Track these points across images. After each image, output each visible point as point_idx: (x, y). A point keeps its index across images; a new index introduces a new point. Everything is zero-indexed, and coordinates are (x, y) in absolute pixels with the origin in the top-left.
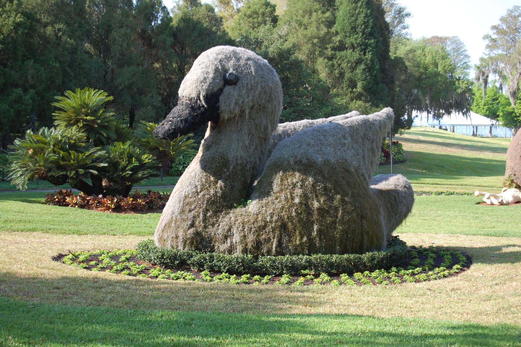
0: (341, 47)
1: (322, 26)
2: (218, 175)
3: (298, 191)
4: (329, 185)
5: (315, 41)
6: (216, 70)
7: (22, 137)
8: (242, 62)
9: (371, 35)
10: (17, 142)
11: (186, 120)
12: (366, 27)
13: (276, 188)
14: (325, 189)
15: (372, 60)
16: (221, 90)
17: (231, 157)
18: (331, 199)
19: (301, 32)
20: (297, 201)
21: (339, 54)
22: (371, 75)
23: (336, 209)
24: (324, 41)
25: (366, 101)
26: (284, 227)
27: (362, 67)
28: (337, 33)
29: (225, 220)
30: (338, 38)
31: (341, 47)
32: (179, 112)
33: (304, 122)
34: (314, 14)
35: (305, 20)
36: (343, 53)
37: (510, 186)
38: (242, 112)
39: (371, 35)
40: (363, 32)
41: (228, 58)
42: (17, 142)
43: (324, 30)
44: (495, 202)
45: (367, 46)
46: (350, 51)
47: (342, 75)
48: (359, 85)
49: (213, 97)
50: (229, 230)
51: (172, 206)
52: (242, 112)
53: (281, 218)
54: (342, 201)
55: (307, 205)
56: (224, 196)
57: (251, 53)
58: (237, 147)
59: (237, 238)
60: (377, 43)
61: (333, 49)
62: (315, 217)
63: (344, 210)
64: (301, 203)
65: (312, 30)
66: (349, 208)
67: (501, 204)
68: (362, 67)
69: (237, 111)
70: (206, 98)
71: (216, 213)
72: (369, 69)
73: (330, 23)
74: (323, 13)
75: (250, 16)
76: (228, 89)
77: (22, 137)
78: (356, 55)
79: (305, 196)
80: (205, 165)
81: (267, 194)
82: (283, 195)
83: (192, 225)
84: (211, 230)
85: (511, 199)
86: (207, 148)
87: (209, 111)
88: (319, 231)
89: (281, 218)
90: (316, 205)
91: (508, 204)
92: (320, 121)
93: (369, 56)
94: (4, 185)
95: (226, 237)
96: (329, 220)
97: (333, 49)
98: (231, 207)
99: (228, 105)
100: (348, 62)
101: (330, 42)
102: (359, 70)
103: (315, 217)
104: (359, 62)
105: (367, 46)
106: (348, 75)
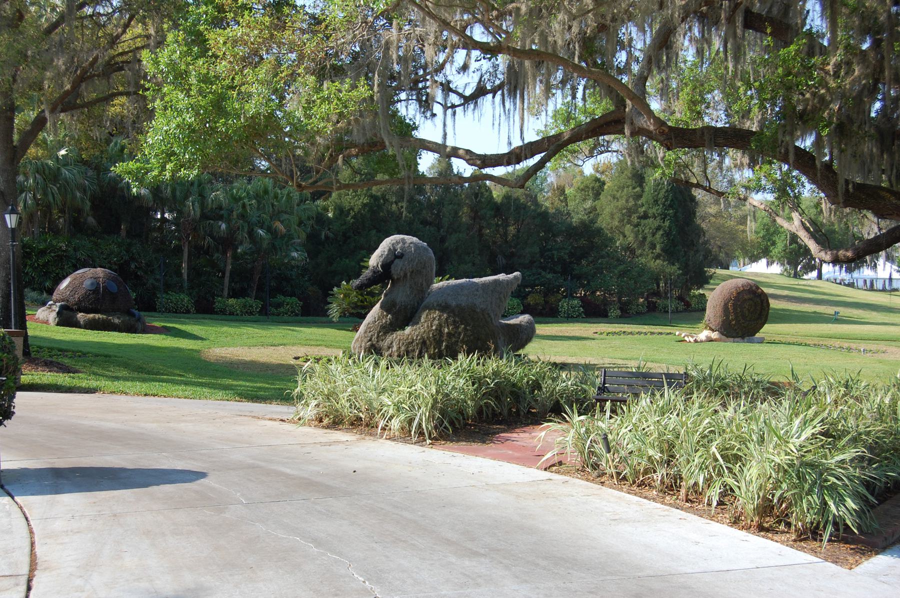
0: (645, 216)
1: (631, 199)
2: (388, 312)
3: (436, 322)
4: (457, 319)
5: (624, 211)
6: (390, 250)
7: (339, 286)
8: (406, 245)
9: (671, 206)
10: (335, 289)
11: (369, 279)
12: (666, 200)
13: (422, 320)
14: (454, 321)
15: (670, 227)
16: (392, 262)
17: (398, 301)
18: (458, 327)
19: (615, 203)
20: (434, 328)
21: (643, 222)
22: (669, 239)
23: (460, 334)
24: (630, 212)
25: (664, 261)
26: (424, 342)
27: (661, 232)
28: (643, 205)
29: (389, 339)
30: (643, 209)
31: (645, 216)
32: (367, 273)
33: (464, 280)
34: (625, 190)
35: (618, 195)
36: (646, 221)
37: (706, 328)
38: (405, 275)
39: (671, 206)
40: (664, 205)
41: (398, 243)
42: (335, 289)
43: (631, 203)
44: (692, 340)
45: (666, 215)
46: (651, 220)
47: (645, 238)
48: (658, 247)
49: (387, 265)
50: (392, 343)
51: (362, 328)
52: (405, 275)
53: (422, 338)
54: (465, 329)
55: (440, 331)
56: (391, 324)
57: (415, 239)
58: (403, 295)
59: (395, 349)
60: (676, 213)
61: (639, 218)
62: (445, 338)
63: (465, 335)
64: (436, 329)
65: (622, 202)
66: (469, 333)
67: (696, 341)
68: (661, 232)
69: (402, 274)
70: (382, 266)
71: (385, 333)
72: (667, 234)
73: (639, 197)
74: (634, 188)
75: (582, 190)
76: (397, 261)
77: (339, 286)
78: (657, 223)
79: (440, 326)
80: (381, 307)
81: (418, 323)
82: (427, 323)
83: (370, 340)
84: (381, 343)
85: (704, 338)
86: (386, 295)
87: (384, 274)
88: (447, 346)
89: (422, 338)
90: (446, 330)
91: (701, 341)
92: (476, 280)
93: (667, 223)
94: (324, 319)
95: (389, 348)
96: (454, 340)
97: (639, 218)
98: (395, 330)
99: (397, 269)
100: (650, 228)
101: (636, 211)
102: (658, 236)
103: (445, 338)
104: (658, 228)
105: (666, 215)
106: (649, 239)
